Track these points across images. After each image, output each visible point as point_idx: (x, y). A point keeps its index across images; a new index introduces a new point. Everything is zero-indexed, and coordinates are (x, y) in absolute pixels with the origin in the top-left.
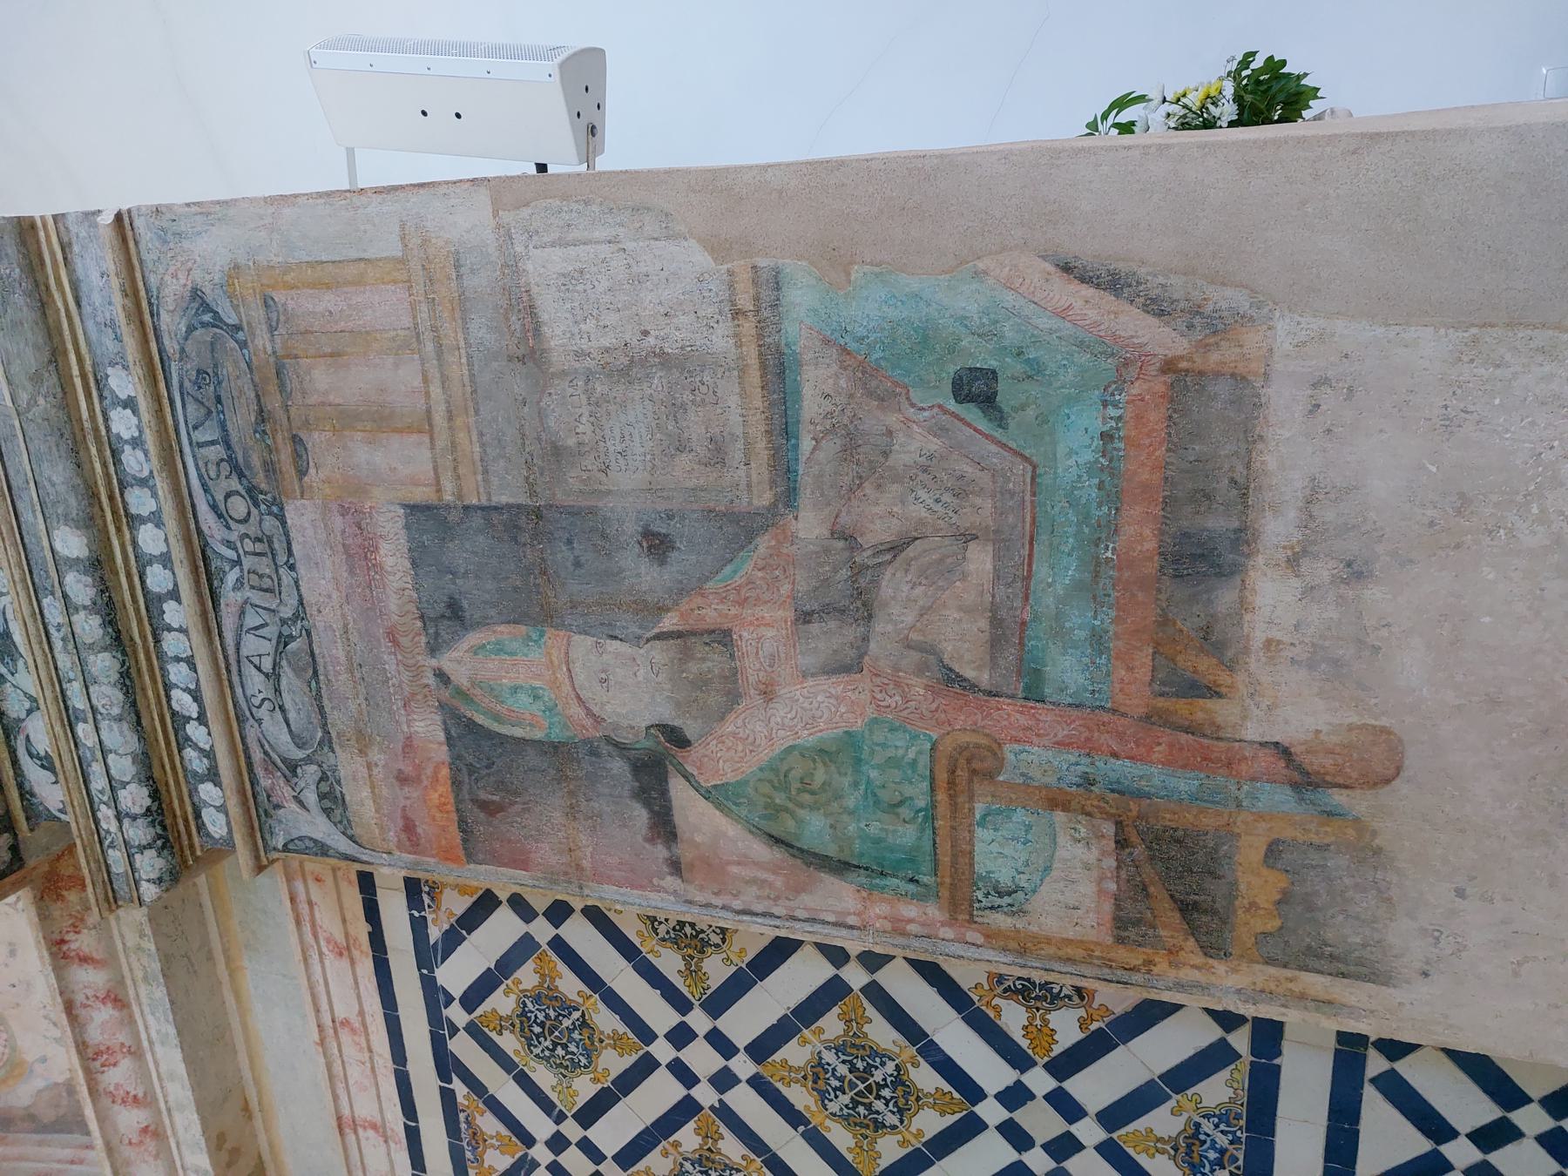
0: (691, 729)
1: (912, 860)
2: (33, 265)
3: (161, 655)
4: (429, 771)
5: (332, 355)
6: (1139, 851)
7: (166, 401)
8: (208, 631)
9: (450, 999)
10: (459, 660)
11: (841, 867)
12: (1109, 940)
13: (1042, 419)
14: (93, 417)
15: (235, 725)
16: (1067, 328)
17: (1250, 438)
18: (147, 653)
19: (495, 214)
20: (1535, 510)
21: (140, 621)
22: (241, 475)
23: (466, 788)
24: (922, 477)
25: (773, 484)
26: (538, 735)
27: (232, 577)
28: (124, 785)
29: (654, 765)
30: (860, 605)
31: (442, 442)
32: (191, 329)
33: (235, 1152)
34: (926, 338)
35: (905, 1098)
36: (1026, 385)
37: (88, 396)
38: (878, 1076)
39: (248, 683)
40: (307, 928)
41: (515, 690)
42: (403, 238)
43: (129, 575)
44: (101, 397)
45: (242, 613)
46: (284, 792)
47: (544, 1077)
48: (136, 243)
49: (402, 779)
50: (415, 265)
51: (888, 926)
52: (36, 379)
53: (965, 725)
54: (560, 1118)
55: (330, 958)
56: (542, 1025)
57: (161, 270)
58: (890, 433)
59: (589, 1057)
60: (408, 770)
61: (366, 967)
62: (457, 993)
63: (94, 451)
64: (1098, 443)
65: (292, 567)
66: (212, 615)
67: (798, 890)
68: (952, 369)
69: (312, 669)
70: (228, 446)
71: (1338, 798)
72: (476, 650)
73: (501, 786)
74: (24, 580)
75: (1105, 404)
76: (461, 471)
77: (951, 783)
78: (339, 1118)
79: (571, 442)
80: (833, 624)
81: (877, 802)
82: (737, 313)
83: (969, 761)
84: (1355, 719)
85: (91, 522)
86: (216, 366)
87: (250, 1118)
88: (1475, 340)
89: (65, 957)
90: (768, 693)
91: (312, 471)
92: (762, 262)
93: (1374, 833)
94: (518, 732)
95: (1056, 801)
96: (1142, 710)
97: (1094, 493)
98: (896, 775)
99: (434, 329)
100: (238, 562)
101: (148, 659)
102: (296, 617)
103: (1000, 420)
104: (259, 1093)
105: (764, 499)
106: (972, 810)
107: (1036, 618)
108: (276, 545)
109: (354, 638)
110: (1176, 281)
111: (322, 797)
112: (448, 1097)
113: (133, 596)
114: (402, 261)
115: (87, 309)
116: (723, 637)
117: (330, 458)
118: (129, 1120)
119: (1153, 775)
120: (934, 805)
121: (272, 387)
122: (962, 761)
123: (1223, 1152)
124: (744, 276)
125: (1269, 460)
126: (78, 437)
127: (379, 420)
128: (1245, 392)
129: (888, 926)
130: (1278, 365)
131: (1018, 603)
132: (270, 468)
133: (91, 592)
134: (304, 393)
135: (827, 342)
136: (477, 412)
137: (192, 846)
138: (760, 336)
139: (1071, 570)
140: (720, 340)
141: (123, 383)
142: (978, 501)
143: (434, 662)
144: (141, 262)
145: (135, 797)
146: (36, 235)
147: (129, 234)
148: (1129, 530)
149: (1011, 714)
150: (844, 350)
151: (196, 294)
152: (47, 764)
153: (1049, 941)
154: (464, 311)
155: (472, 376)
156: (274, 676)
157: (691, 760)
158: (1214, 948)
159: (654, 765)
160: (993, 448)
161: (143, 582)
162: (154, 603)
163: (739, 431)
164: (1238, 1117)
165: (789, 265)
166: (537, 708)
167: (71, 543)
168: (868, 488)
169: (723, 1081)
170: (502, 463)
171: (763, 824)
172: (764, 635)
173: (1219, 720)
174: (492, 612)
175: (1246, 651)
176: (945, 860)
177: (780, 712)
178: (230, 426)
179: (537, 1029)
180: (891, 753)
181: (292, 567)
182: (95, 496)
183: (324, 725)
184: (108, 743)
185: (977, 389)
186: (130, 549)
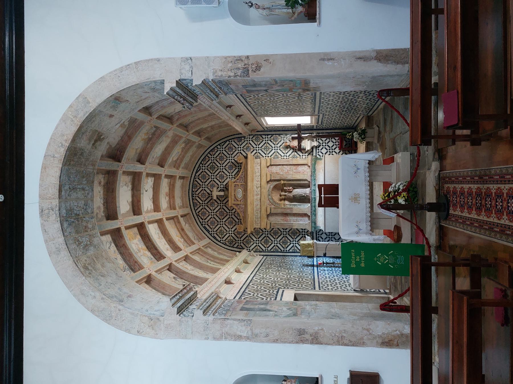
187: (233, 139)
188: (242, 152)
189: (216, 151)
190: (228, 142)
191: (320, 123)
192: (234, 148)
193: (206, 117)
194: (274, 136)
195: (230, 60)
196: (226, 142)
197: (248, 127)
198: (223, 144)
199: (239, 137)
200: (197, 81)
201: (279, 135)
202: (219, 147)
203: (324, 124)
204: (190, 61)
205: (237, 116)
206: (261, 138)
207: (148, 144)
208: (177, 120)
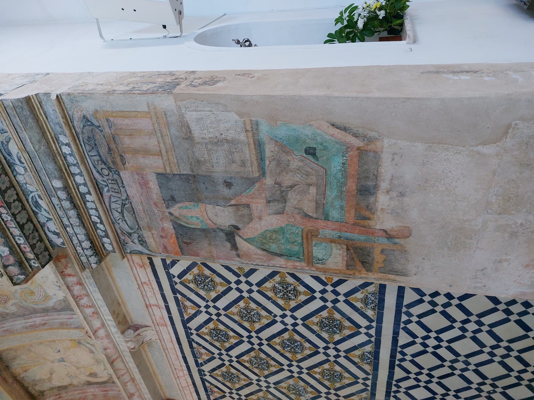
0: (240, 226)
1: (298, 254)
2: (32, 109)
3: (87, 208)
4: (170, 235)
5: (129, 135)
6: (352, 251)
7: (79, 145)
8: (101, 203)
9: (174, 277)
10: (175, 210)
11: (281, 255)
12: (345, 269)
13: (328, 159)
14: (57, 149)
15: (112, 225)
16: (333, 139)
17: (378, 164)
18: (83, 208)
19: (176, 102)
20: (443, 182)
21: (79, 200)
22: (105, 164)
23: (180, 239)
24: (297, 171)
25: (259, 171)
26: (199, 227)
27: (106, 189)
28: (83, 242)
29: (231, 234)
30: (283, 199)
31: (165, 158)
32: (84, 126)
33: (118, 314)
34: (297, 140)
35: (296, 293)
36: (323, 151)
37: (54, 143)
38: (289, 289)
39: (114, 214)
40: (131, 262)
41: (192, 217)
42: (148, 106)
43: (74, 189)
44: (58, 143)
45: (110, 198)
46: (128, 240)
47: (202, 293)
48: (64, 103)
49: (162, 237)
50: (153, 114)
51: (292, 267)
52: (39, 142)
53: (309, 225)
54: (207, 301)
55: (138, 268)
56: (201, 281)
57: (72, 110)
58: (289, 161)
59: (214, 288)
60: (163, 235)
61: (149, 270)
62: (176, 275)
63: (59, 158)
64: (341, 165)
65: (124, 187)
66: (101, 199)
67: (270, 260)
68: (304, 147)
69: (133, 211)
70: (100, 157)
71: (397, 240)
72: (180, 208)
73: (190, 238)
74: (45, 194)
75: (343, 156)
76: (172, 165)
77: (307, 238)
78: (146, 305)
79: (202, 159)
80: (276, 204)
81: (289, 242)
82: (247, 131)
83: (311, 233)
84: (401, 225)
85: (62, 177)
86: (93, 136)
87: (120, 305)
88: (430, 146)
89: (64, 275)
90: (260, 218)
91: (127, 164)
92: (253, 119)
93: (405, 247)
94: (193, 227)
95: (332, 241)
96: (352, 223)
97: (341, 176)
98: (294, 236)
99: (160, 130)
100: (107, 186)
101: (83, 209)
102: (126, 199)
104: (122, 300)
105: (257, 175)
106: (312, 243)
107: (327, 203)
108: (118, 181)
109: (144, 204)
110: (360, 129)
111: (139, 241)
112: (176, 299)
113: (77, 194)
114: (149, 113)
115: (50, 120)
116: (248, 206)
117: (131, 161)
118: (89, 311)
119: (355, 236)
120: (303, 242)
121: (112, 142)
122: (309, 233)
123: (373, 301)
124: (248, 123)
125: (382, 170)
126: (54, 155)
129: (292, 267)
130: (385, 150)
131: (322, 199)
132: (114, 163)
133: (66, 195)
134: (122, 144)
135: (271, 139)
136: (175, 151)
137: (103, 253)
138: (253, 137)
139: (335, 193)
140: (242, 137)
141: (63, 139)
142: (312, 177)
143: (168, 210)
144: (66, 108)
145: (86, 244)
146: (31, 101)
147: (61, 101)
148: (349, 184)
150: (276, 141)
151: (84, 117)
152: (55, 233)
153: (331, 269)
154: (168, 126)
155: (172, 142)
156: (122, 213)
157: (241, 233)
158: (369, 270)
159: (231, 234)
160: (315, 165)
161: (79, 190)
162: (83, 195)
163: (249, 159)
164: (376, 293)
165: (260, 120)
166: (198, 221)
167: (58, 184)
168: (284, 173)
169: (250, 291)
170: (183, 164)
171: (260, 246)
172: (258, 205)
173: (370, 225)
174: (184, 199)
175: (377, 210)
176: (306, 253)
177: (263, 223)
178: (100, 152)
179: (199, 282)
180: (292, 231)
181: (124, 187)
182: (61, 170)
183: (138, 225)
184: (77, 232)
185: (311, 152)
186: (73, 182)
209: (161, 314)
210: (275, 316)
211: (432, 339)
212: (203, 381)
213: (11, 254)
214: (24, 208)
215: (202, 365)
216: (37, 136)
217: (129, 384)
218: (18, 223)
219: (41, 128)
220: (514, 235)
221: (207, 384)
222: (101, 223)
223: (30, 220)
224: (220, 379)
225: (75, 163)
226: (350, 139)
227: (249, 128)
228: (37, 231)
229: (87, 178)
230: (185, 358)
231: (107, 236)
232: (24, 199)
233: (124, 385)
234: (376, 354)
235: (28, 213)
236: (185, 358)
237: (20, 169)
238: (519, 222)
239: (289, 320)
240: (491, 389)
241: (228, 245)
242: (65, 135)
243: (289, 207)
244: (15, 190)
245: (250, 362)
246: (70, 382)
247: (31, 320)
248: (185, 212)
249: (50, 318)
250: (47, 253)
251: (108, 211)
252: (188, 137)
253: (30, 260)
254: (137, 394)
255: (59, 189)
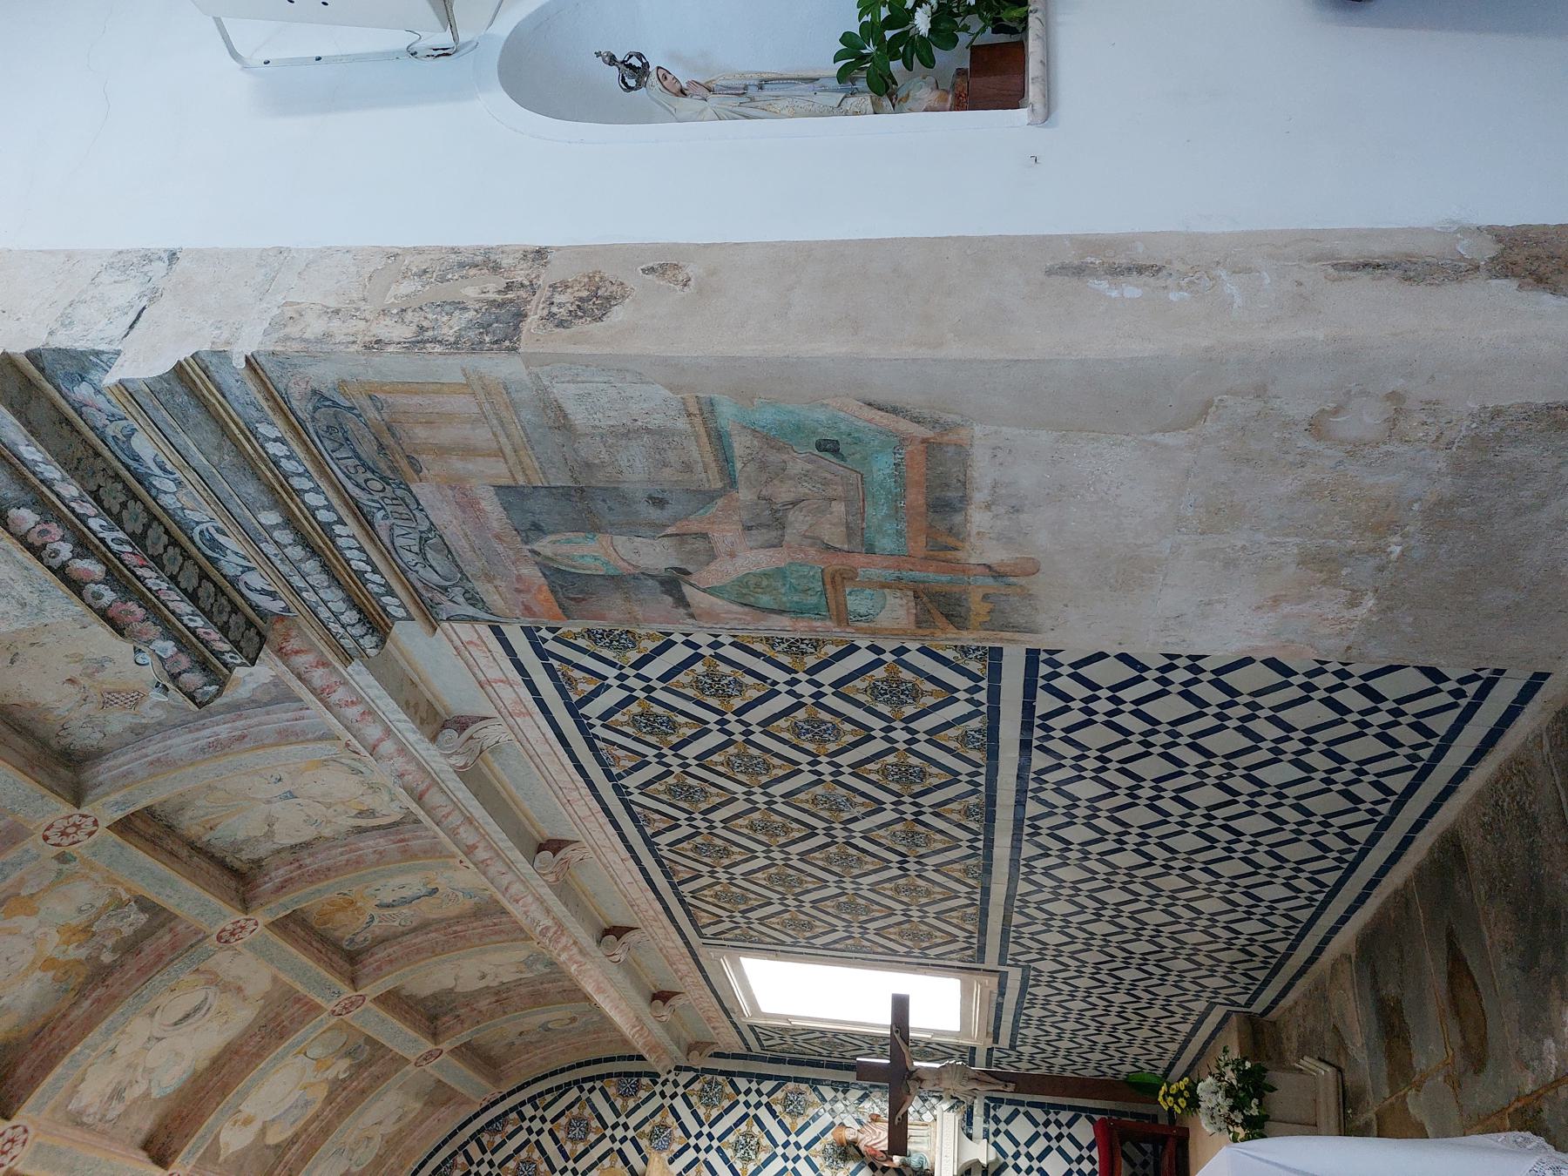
0: (690, 568)
8: (372, 540)
10: (545, 546)
11: (781, 612)
14: (256, 451)
29: (672, 583)
32: (316, 409)
37: (248, 440)
45: (391, 529)
46: (438, 597)
47: (608, 654)
49: (518, 591)
52: (219, 448)
53: (836, 563)
54: (622, 667)
70: (359, 459)
71: (1012, 579)
73: (581, 592)
85: (278, 504)
102: (430, 530)
103: (843, 459)
105: (719, 485)
115: (230, 398)
117: (433, 467)
118: (352, 712)
121: (387, 434)
125: (975, 473)
126: (252, 464)
127: (469, 451)
128: (963, 453)
132: (394, 470)
140: (682, 424)
145: (350, 616)
149: (859, 559)
152: (263, 592)
159: (672, 583)
165: (715, 396)
167: (271, 518)
172: (726, 534)
176: (833, 605)
177: (739, 562)
185: (829, 447)
187: (601, 1077)
188: (628, 1148)
189: (510, 1129)
190: (574, 1093)
191: (1004, 1042)
192: (595, 1123)
193: (458, 919)
194: (791, 1085)
195: (417, 264)
196: (563, 1089)
197: (666, 1014)
198: (549, 1098)
199: (627, 1073)
200: (143, 361)
201: (814, 1083)
202: (528, 1111)
203: (1027, 1050)
204: (159, 267)
205: (607, 932)
206: (729, 1089)
207: (81, 994)
208: (281, 888)
209: (514, 694)
210: (775, 683)
211: (1103, 701)
212: (627, 806)
213: (180, 650)
214: (186, 556)
215: (620, 776)
216: (210, 437)
217: (461, 830)
218: (185, 591)
219: (216, 419)
220: (1230, 563)
221: (636, 809)
222: (375, 571)
223: (203, 576)
224: (664, 797)
225: (301, 470)
226: (905, 426)
227: (694, 409)
228: (224, 594)
229: (331, 494)
230: (580, 768)
231: (391, 592)
232: (183, 539)
233: (453, 833)
234: (992, 731)
235: (196, 563)
236: (580, 768)
237: (163, 483)
238: (1239, 544)
239: (805, 689)
240: (1224, 771)
241: (669, 600)
242: (272, 424)
243: (791, 535)
244: (161, 523)
245: (728, 763)
246: (315, 834)
247: (207, 732)
248: (565, 549)
249: (249, 722)
250: (253, 631)
251: (390, 553)
252: (562, 423)
253: (223, 653)
254: (482, 845)
255: (276, 527)
